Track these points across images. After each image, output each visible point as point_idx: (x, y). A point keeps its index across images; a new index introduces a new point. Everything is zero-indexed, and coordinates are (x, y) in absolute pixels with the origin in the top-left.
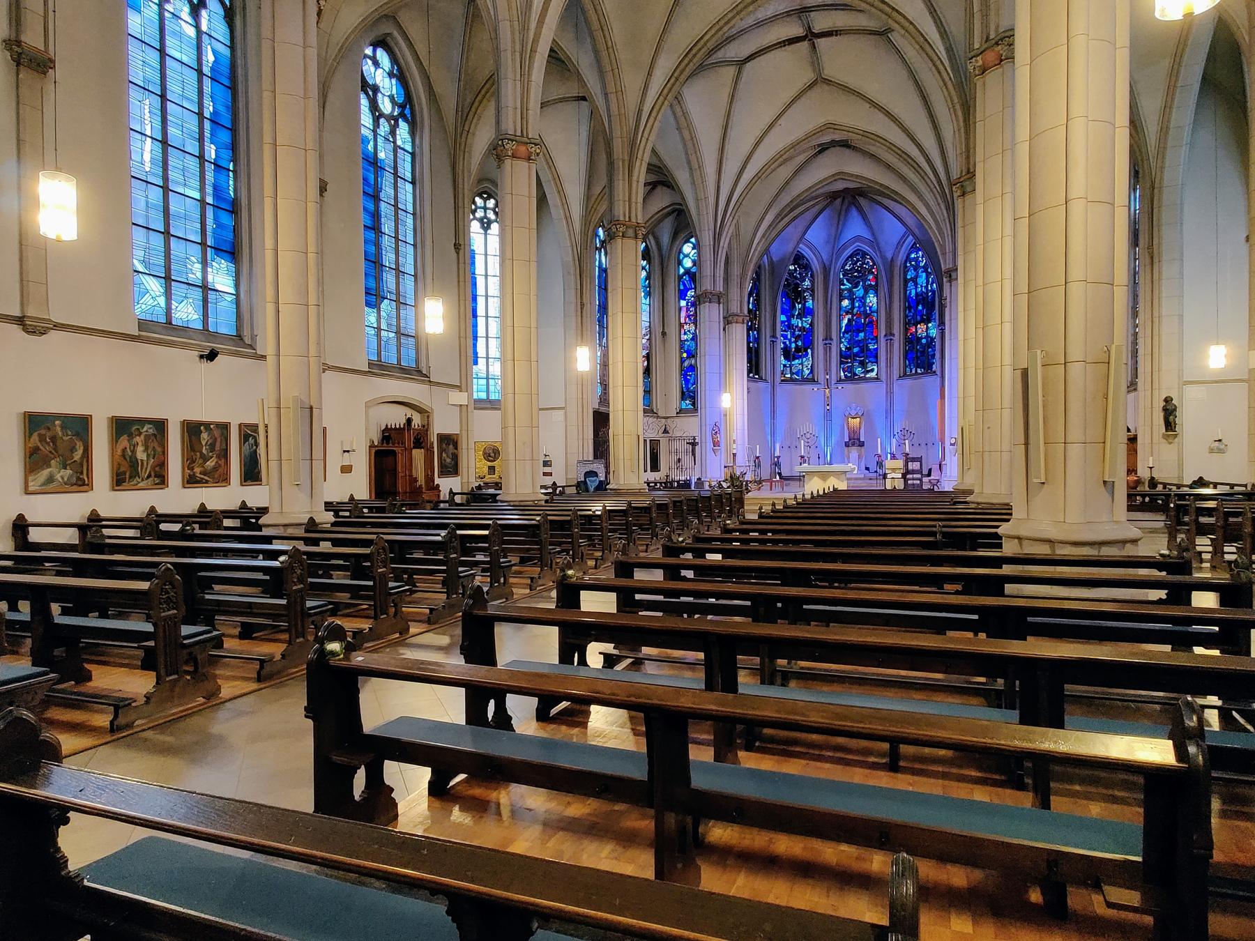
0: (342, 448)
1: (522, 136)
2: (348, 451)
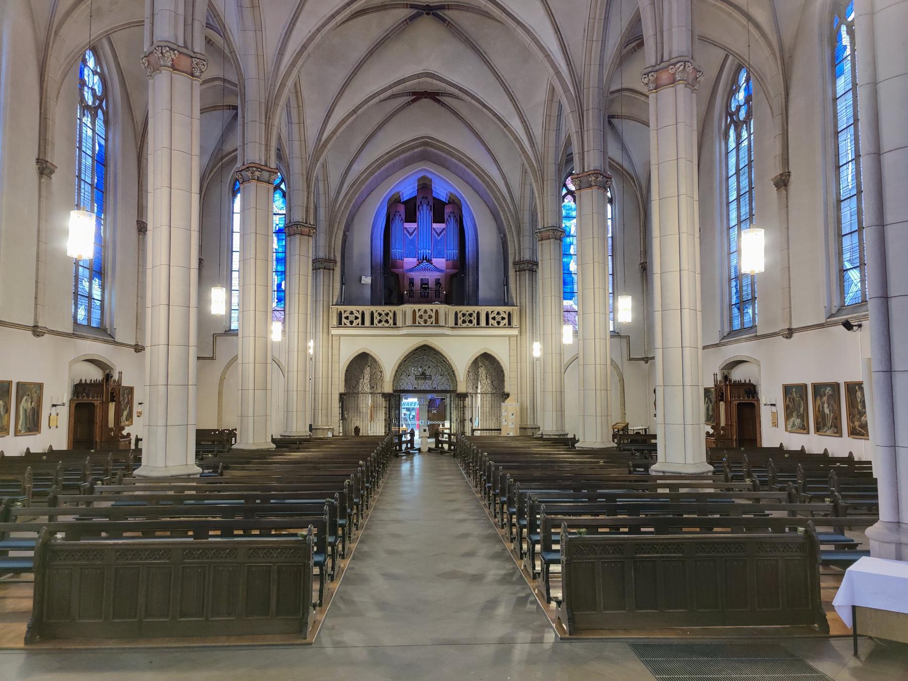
0: (51, 402)
1: (186, 47)
2: (772, 405)
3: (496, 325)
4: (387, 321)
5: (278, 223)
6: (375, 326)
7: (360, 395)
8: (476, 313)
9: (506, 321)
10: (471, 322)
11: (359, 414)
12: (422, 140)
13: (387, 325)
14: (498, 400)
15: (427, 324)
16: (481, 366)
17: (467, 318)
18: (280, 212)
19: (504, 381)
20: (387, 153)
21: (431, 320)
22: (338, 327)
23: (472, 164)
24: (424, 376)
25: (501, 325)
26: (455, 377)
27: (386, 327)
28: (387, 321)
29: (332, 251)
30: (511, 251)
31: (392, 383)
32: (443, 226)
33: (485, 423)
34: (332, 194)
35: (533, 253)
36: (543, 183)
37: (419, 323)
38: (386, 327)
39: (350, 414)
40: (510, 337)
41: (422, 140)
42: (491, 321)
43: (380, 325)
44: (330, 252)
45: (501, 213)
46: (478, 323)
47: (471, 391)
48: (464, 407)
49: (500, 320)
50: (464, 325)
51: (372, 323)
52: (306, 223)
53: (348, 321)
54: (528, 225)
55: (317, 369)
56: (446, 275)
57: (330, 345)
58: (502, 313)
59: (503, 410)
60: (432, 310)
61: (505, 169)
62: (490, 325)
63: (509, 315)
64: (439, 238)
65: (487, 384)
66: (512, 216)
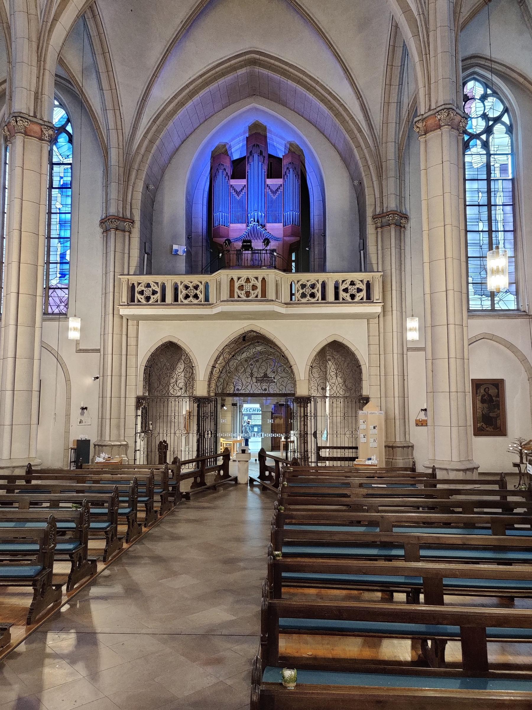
3: (349, 299)
4: (196, 296)
5: (62, 175)
6: (179, 303)
7: (172, 399)
8: (320, 283)
9: (363, 294)
10: (313, 295)
11: (169, 425)
12: (247, 56)
13: (196, 301)
14: (354, 405)
15: (250, 298)
16: (330, 360)
17: (308, 291)
18: (66, 161)
19: (361, 379)
20: (201, 76)
21: (256, 292)
22: (128, 305)
23: (314, 85)
24: (265, 378)
25: (357, 299)
26: (294, 375)
27: (194, 304)
28: (196, 296)
29: (128, 207)
30: (369, 200)
31: (207, 383)
32: (279, 181)
33: (335, 439)
34: (127, 130)
35: (401, 202)
36: (428, 36)
37: (239, 297)
38: (194, 304)
39: (158, 425)
40: (368, 317)
41: (247, 56)
42: (342, 294)
43: (186, 302)
44: (124, 208)
45: (355, 151)
46: (324, 297)
47: (314, 394)
48: (305, 416)
49: (354, 292)
50: (304, 300)
51: (176, 299)
52: (35, 116)
53: (142, 297)
54: (393, 162)
55: (106, 363)
56: (283, 244)
57: (124, 332)
58: (357, 282)
59: (361, 421)
60: (257, 278)
61: (360, 83)
62: (341, 300)
63: (368, 285)
64: (274, 198)
65: (337, 383)
66: (370, 151)
